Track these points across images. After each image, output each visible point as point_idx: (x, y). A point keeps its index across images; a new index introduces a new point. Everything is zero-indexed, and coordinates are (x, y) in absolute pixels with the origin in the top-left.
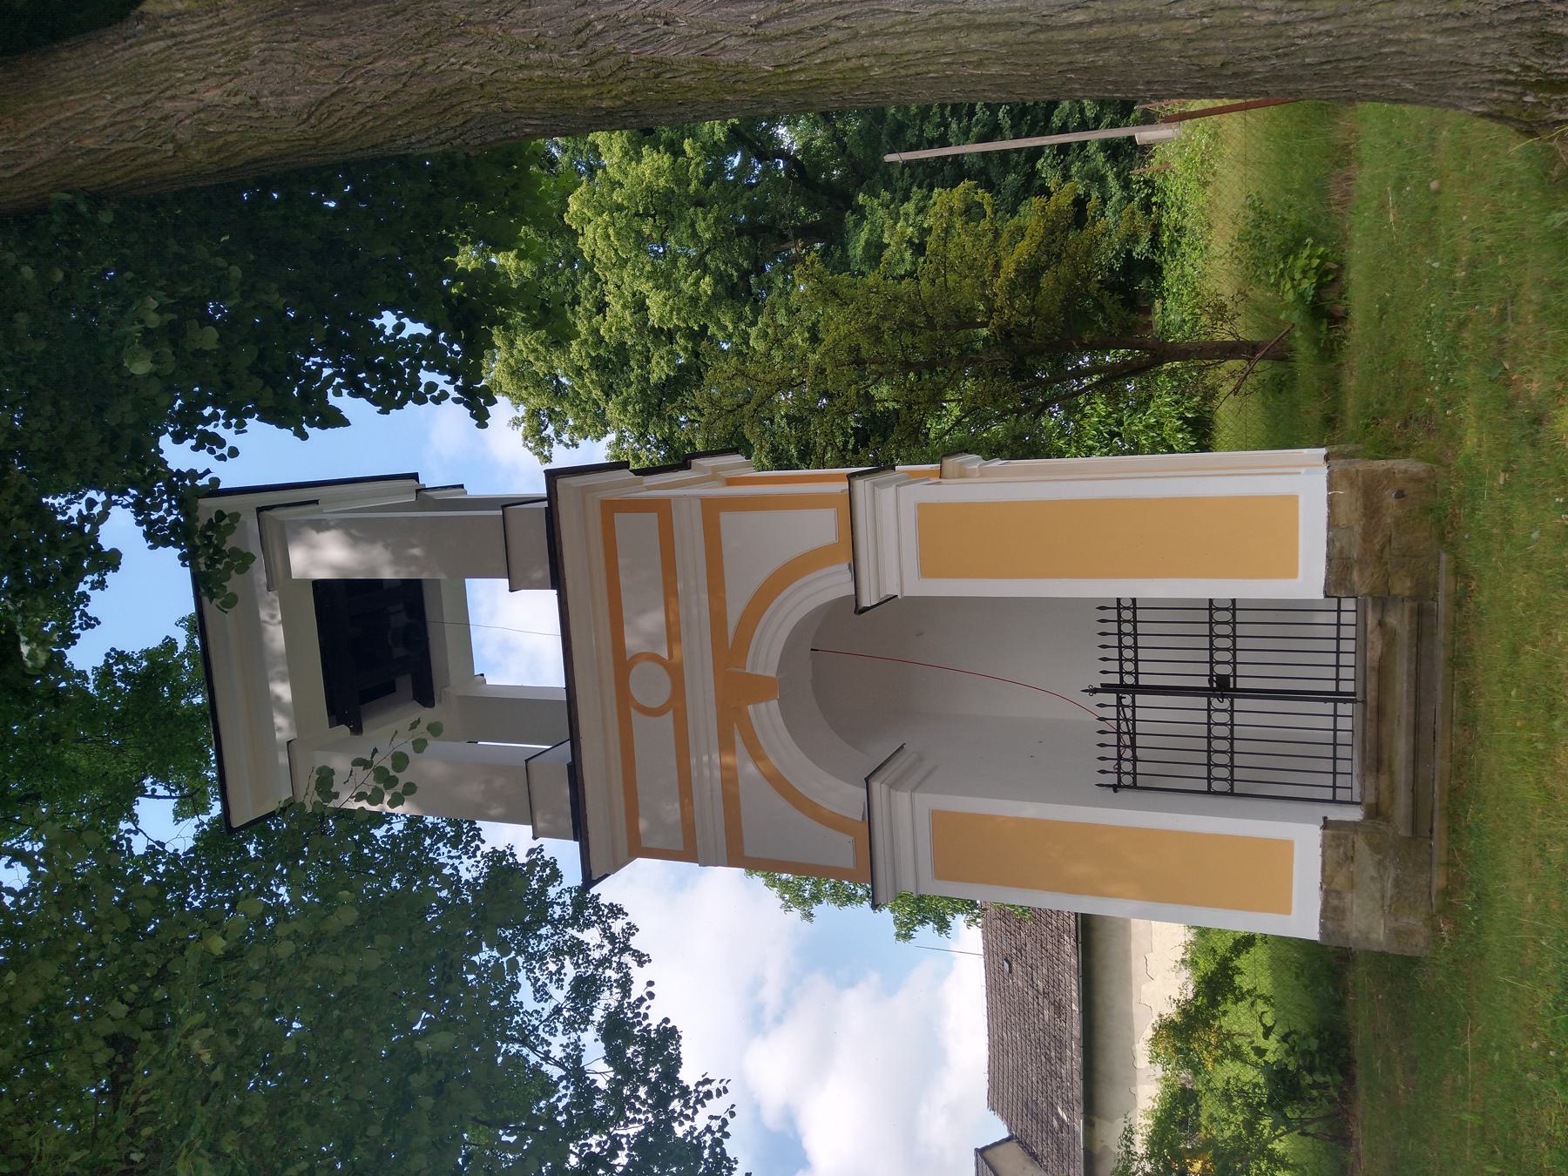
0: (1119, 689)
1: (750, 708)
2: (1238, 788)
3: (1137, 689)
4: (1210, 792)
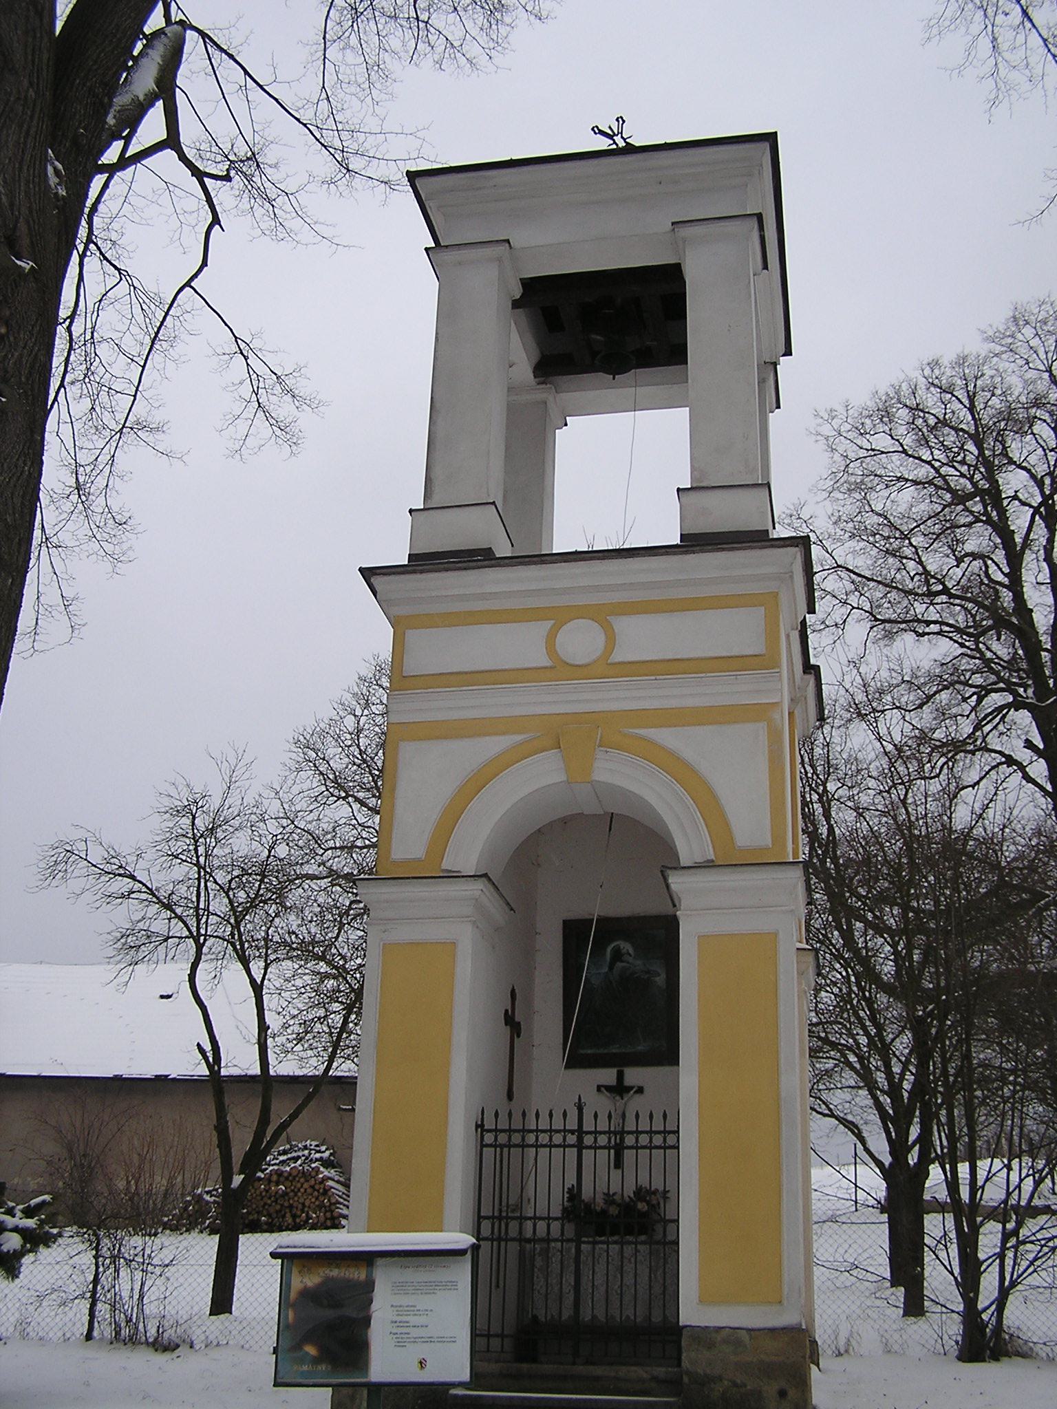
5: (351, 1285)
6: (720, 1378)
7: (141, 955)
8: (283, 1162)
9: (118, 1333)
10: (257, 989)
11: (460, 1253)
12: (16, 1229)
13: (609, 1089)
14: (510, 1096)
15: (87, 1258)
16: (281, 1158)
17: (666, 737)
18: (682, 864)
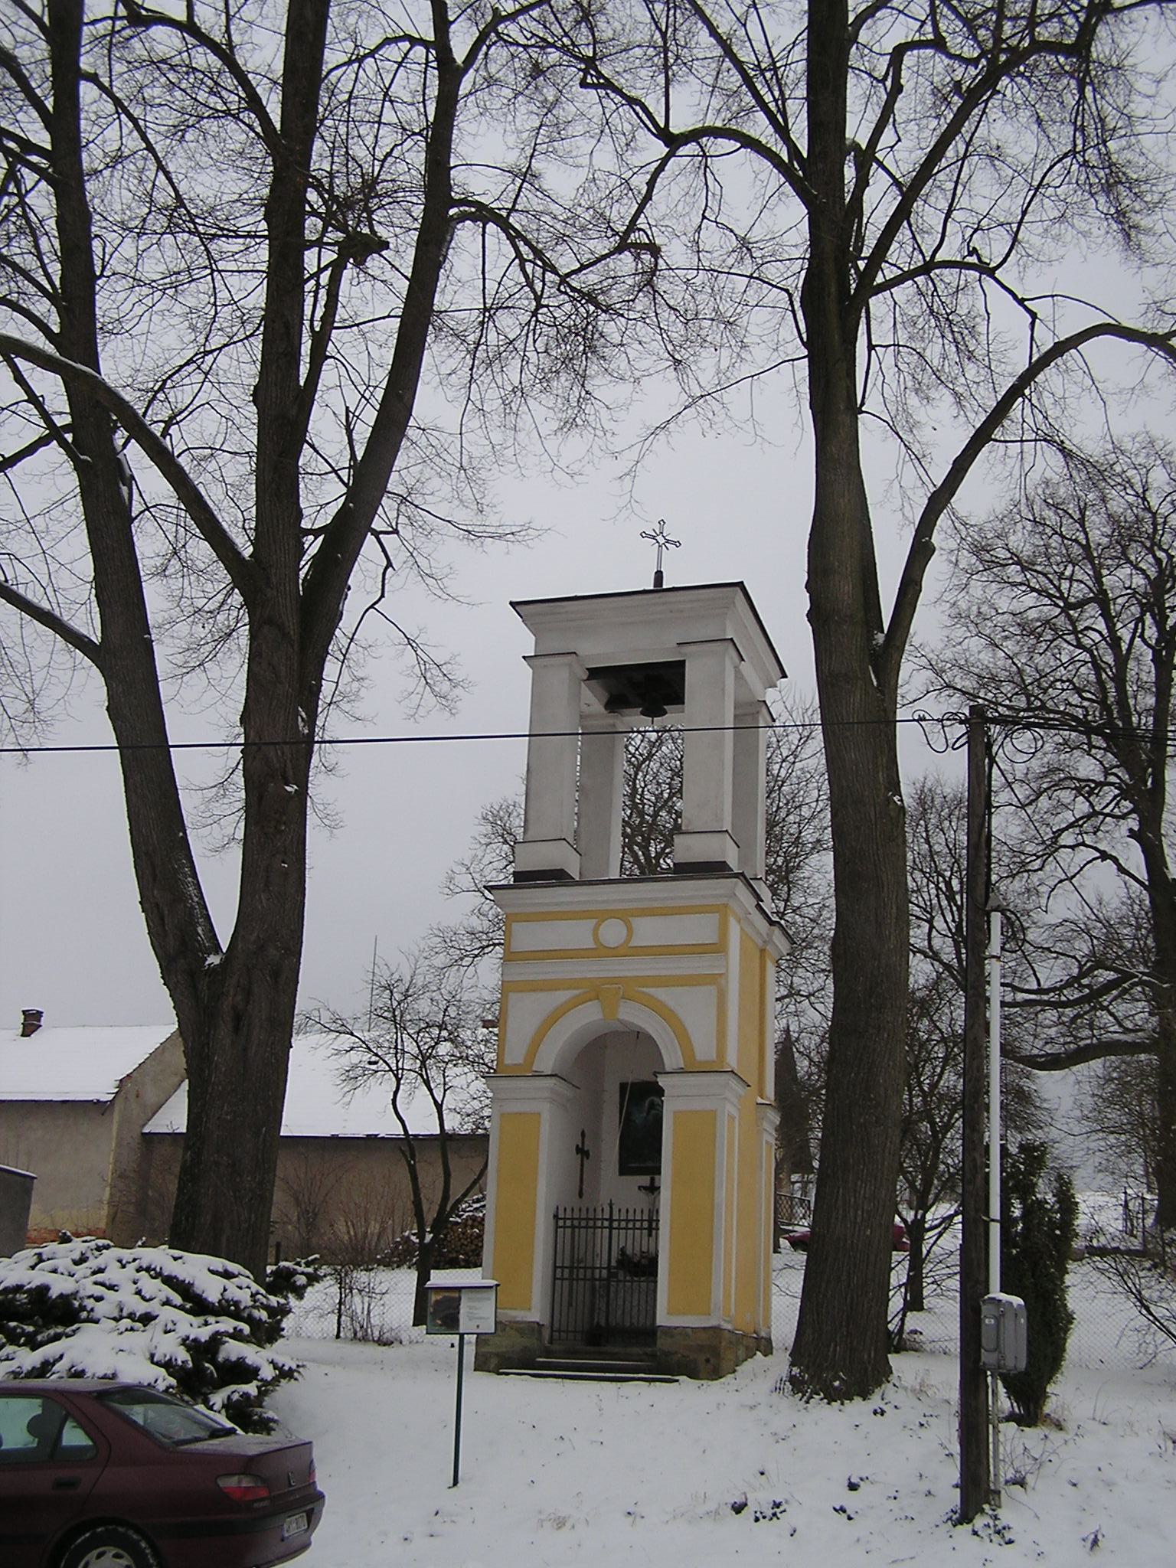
2: (558, 1282)
4: (555, 1267)
5: (453, 1299)
6: (676, 1353)
7: (359, 1083)
8: (477, 1209)
9: (355, 1334)
10: (439, 1107)
11: (491, 1287)
12: (302, 1273)
13: (645, 1188)
15: (336, 1289)
16: (476, 1205)
17: (660, 993)
18: (668, 1069)
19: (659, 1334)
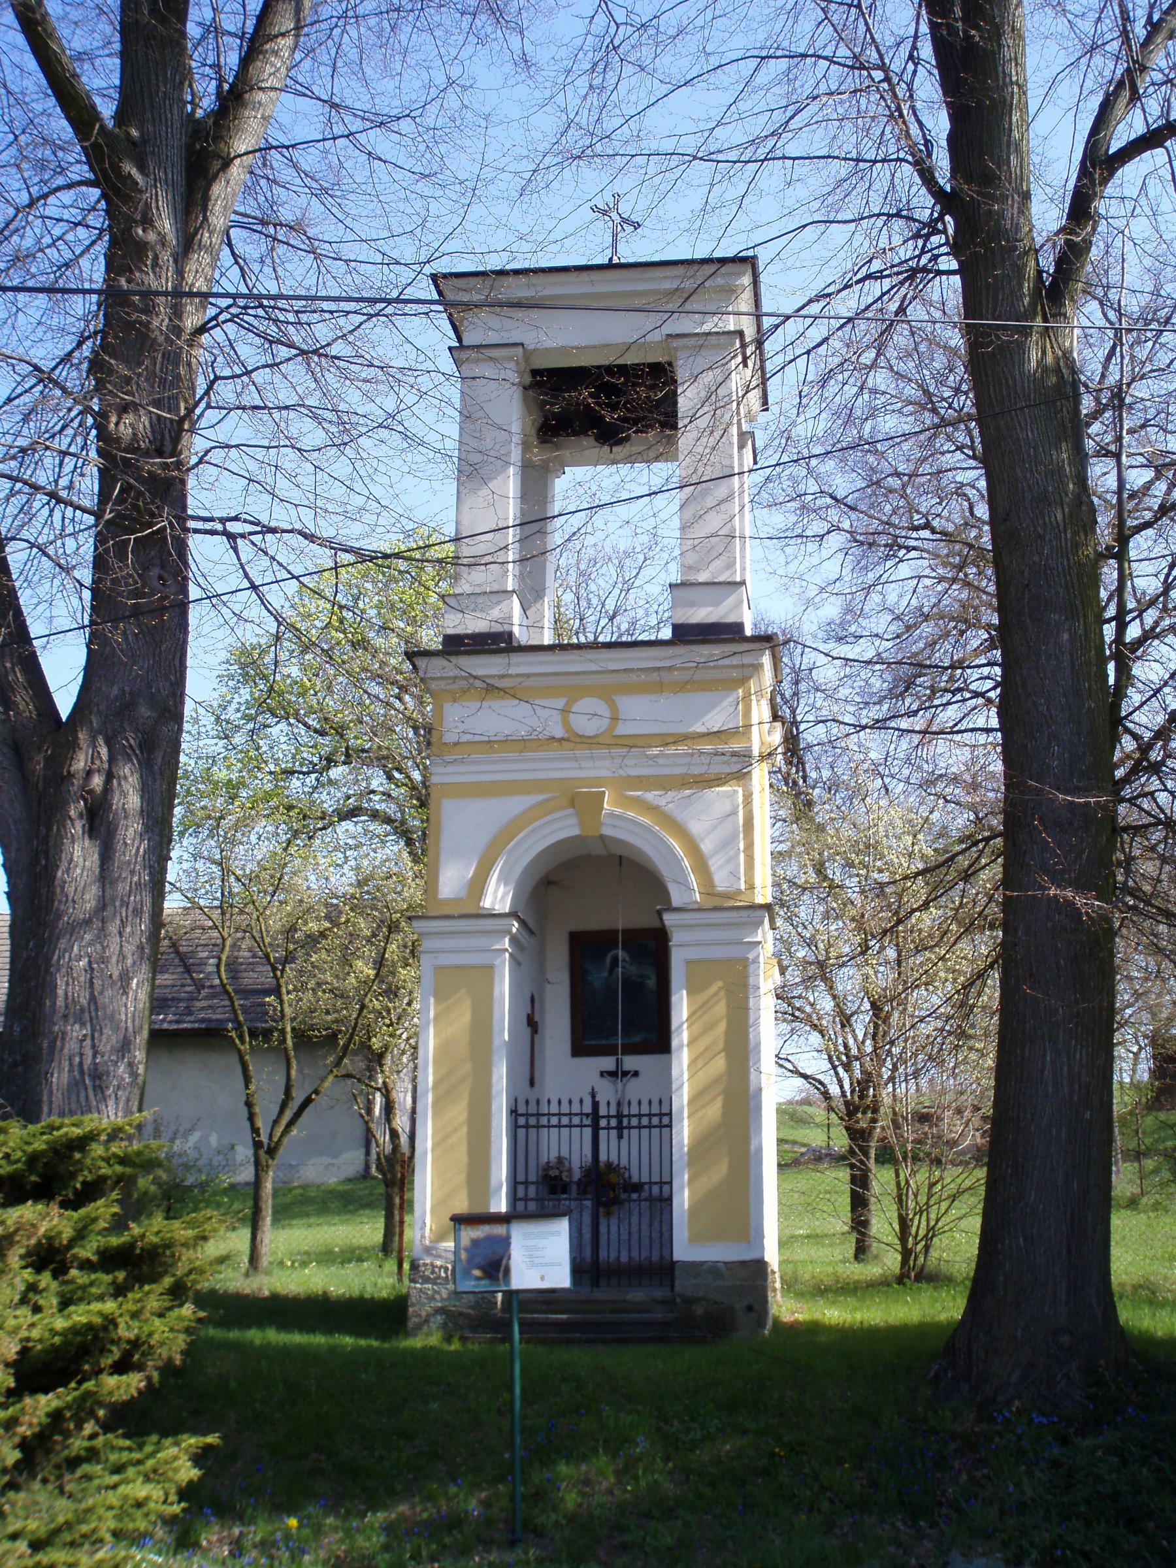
0: (595, 1115)
1: (464, 991)
3: (596, 1129)
14: (532, 1083)
19: (677, 1272)
